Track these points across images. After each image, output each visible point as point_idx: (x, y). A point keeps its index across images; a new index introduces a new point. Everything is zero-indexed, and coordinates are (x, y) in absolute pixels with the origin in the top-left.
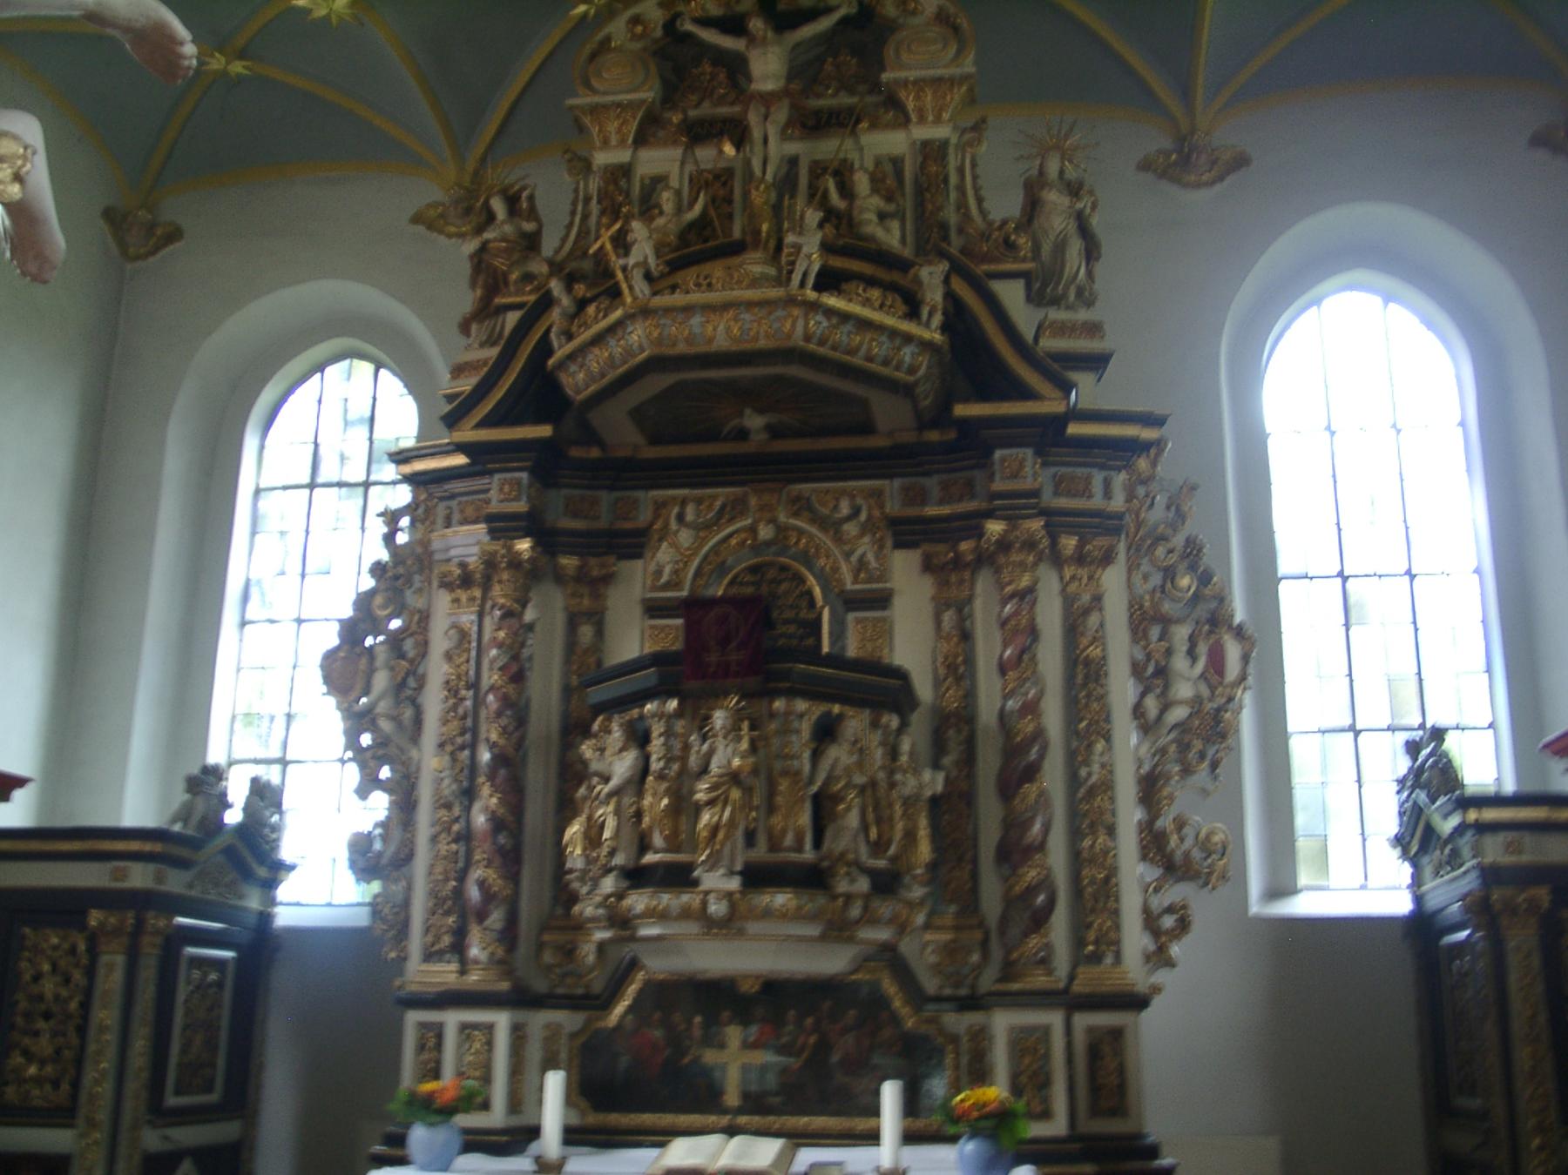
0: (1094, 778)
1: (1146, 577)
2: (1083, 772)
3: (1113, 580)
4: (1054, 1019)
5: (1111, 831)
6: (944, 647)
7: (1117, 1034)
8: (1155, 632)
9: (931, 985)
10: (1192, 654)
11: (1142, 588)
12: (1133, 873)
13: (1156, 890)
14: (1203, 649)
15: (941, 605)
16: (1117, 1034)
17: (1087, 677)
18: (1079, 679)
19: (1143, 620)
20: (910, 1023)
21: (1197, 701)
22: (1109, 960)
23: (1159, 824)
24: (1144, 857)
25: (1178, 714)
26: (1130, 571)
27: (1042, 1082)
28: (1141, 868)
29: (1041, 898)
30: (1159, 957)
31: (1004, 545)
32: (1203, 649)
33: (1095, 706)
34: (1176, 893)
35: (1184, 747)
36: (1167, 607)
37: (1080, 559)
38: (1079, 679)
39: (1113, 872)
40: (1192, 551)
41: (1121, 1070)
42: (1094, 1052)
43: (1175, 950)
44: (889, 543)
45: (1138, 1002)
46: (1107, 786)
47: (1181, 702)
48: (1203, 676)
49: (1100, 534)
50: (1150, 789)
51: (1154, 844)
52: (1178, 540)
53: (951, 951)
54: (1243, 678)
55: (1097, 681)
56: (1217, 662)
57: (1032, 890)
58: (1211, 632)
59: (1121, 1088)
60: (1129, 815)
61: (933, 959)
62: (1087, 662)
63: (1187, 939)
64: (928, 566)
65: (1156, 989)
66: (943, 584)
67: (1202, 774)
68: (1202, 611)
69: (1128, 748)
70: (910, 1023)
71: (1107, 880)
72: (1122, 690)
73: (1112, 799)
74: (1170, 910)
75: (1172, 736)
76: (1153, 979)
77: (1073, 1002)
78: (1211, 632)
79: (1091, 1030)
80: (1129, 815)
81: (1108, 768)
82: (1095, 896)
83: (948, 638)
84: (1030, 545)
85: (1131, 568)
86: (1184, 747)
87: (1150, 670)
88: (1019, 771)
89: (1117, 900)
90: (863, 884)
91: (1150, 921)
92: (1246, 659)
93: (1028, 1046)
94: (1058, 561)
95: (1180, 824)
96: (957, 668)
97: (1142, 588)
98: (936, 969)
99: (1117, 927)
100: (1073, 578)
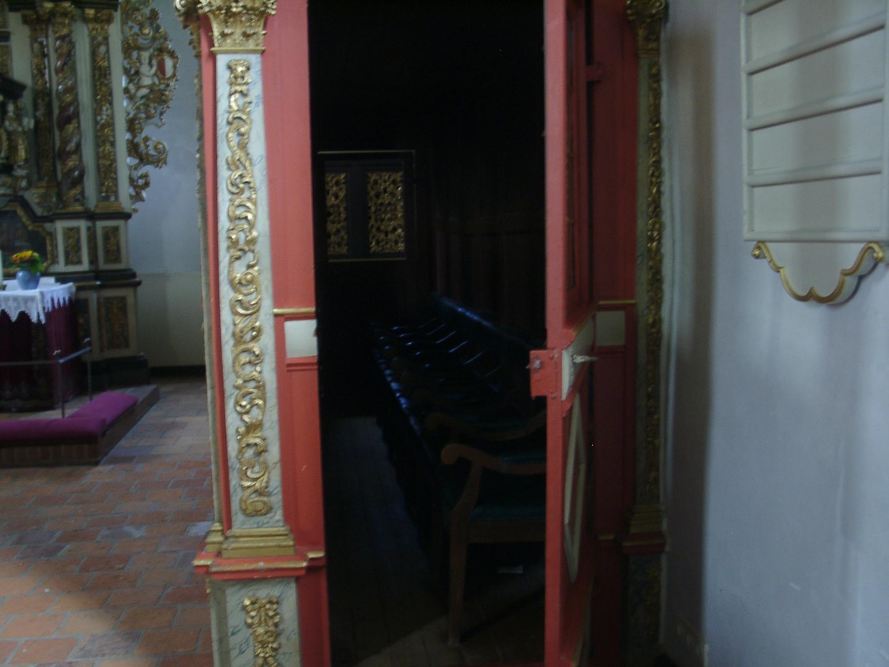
0: (103, 121)
1: (131, 28)
2: (99, 118)
3: (115, 31)
4: (82, 225)
5: (113, 144)
6: (36, 60)
7: (116, 229)
8: (135, 54)
9: (39, 211)
10: (150, 64)
11: (128, 33)
12: (125, 162)
13: (136, 169)
14: (154, 62)
15: (34, 39)
16: (116, 229)
17: (100, 76)
18: (97, 77)
19: (128, 49)
20: (30, 228)
21: (151, 88)
22: (113, 199)
23: (136, 140)
24: (130, 155)
25: (144, 91)
26: (122, 26)
27: (77, 248)
28: (129, 160)
29: (76, 173)
30: (137, 197)
31: (52, 14)
32: (154, 62)
33: (104, 89)
34: (148, 169)
35: (147, 106)
36: (140, 41)
37: (96, 20)
38: (97, 77)
39: (114, 161)
40: (154, 15)
41: (118, 245)
42: (106, 237)
43: (144, 194)
44: (7, 8)
45: (127, 216)
46: (110, 124)
47: (144, 87)
48: (155, 74)
49: (103, 9)
50: (132, 125)
51: (133, 149)
52: (147, 11)
53: (44, 197)
54: (174, 75)
55: (105, 76)
56: (161, 68)
57: (72, 170)
58: (158, 55)
59: (118, 250)
60: (122, 137)
61: (37, 200)
62: (100, 68)
63: (148, 189)
64: (25, 21)
65: (135, 211)
66: (34, 30)
67: (156, 120)
68: (157, 44)
69: (122, 106)
70: (30, 228)
71: (111, 165)
72: (120, 81)
73: (113, 130)
74: (141, 177)
75: (142, 101)
76: (133, 207)
77: (91, 216)
78: (158, 55)
79: (104, 228)
80: (122, 137)
81: (112, 116)
82: (107, 171)
83: (37, 56)
84: (65, 14)
85: (124, 22)
86: (147, 106)
87: (133, 72)
88: (69, 116)
89: (116, 173)
90: (392, 186)
91: (132, 181)
92: (175, 67)
93: (72, 234)
94: (86, 20)
95: (146, 139)
96: (39, 72)
97: (128, 33)
98: (39, 204)
99: (116, 185)
100: (93, 29)
